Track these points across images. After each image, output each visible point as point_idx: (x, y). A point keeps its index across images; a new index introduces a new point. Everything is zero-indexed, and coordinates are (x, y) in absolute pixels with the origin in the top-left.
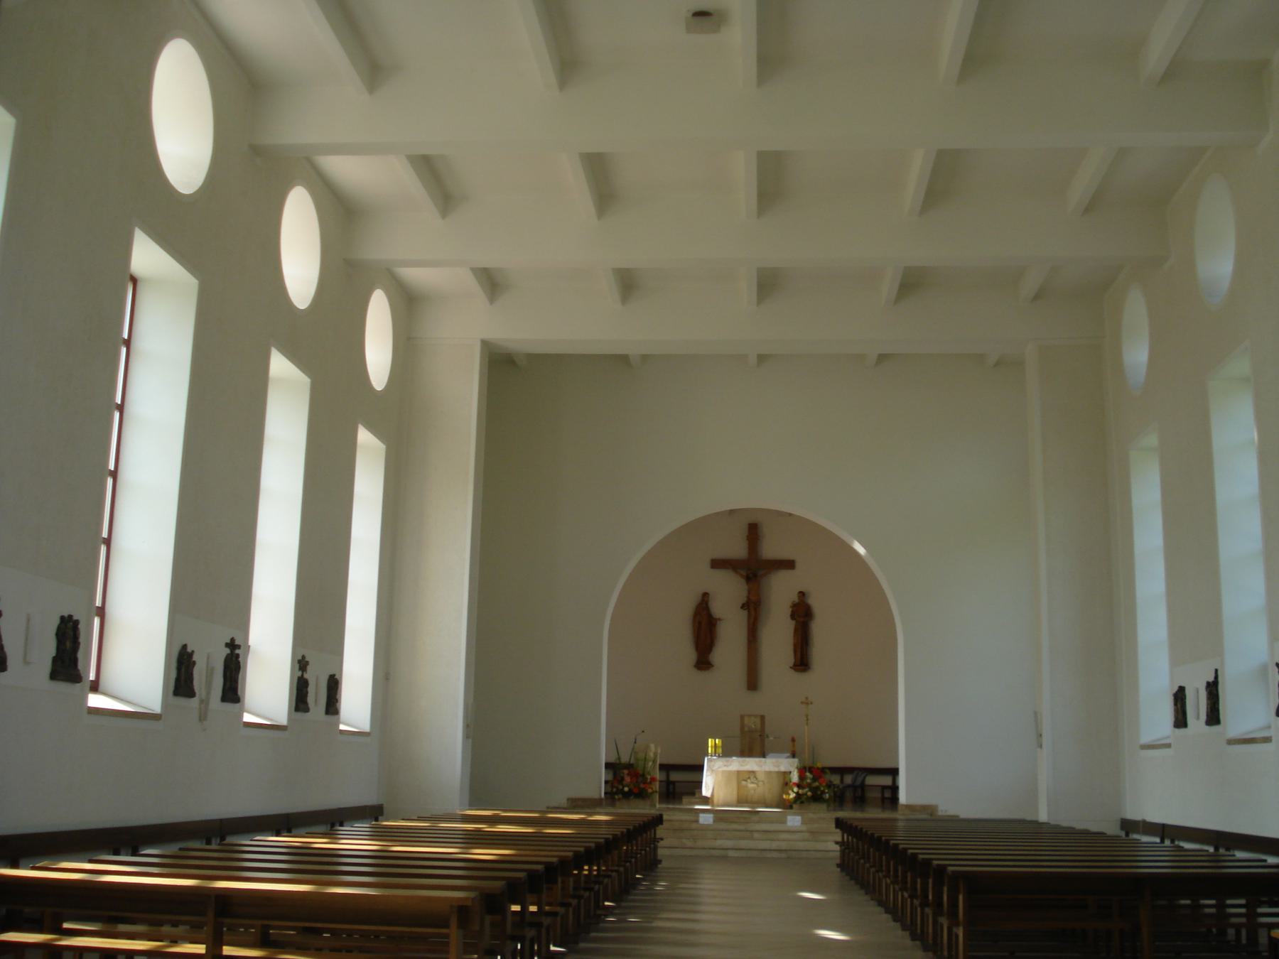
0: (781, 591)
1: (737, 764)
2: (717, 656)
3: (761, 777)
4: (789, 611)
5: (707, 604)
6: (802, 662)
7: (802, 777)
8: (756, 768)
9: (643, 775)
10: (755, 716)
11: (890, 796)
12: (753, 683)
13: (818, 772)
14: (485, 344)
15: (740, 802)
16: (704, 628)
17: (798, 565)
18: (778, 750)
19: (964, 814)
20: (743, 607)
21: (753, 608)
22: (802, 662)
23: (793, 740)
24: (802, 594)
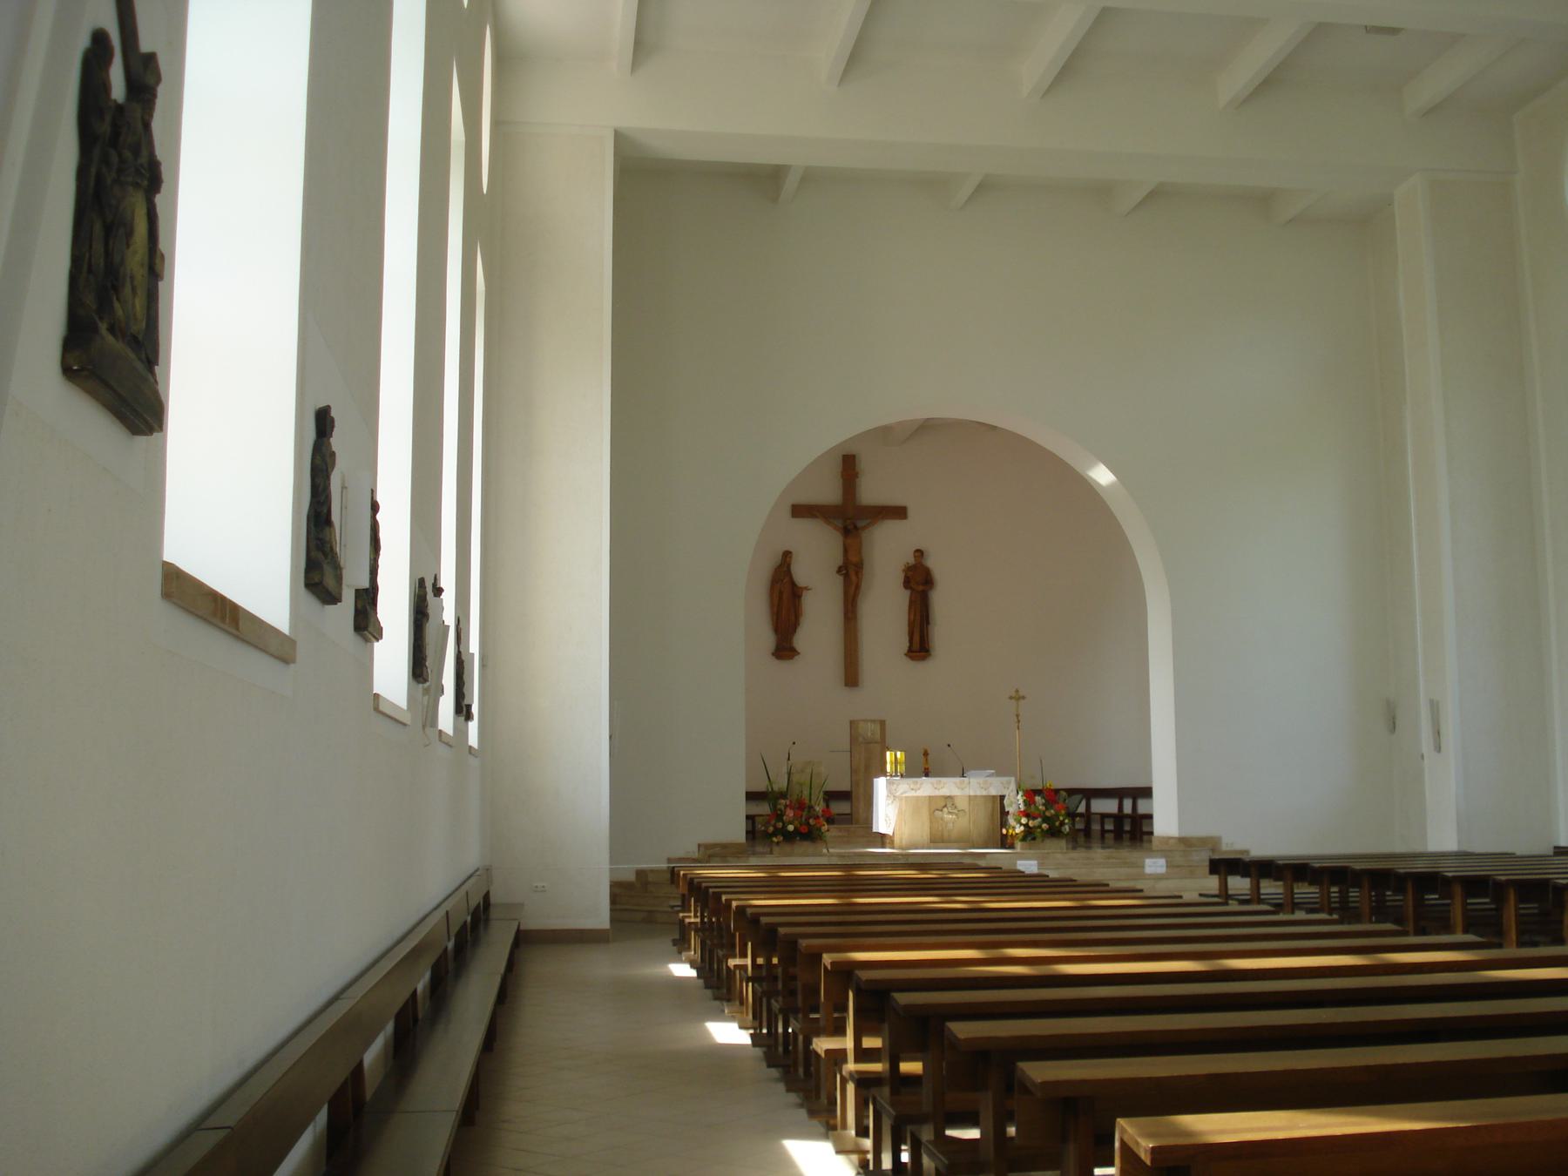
0: (887, 550)
1: (927, 787)
2: (801, 640)
3: (962, 804)
4: (900, 577)
5: (789, 566)
6: (920, 647)
7: (1029, 801)
8: (955, 792)
9: (811, 807)
10: (873, 721)
11: (1132, 829)
12: (851, 678)
13: (1052, 795)
14: (621, 140)
15: (935, 840)
16: (785, 601)
17: (910, 513)
18: (980, 765)
19: (1520, 850)
20: (839, 571)
21: (852, 572)
22: (920, 647)
23: (926, 754)
24: (919, 553)
